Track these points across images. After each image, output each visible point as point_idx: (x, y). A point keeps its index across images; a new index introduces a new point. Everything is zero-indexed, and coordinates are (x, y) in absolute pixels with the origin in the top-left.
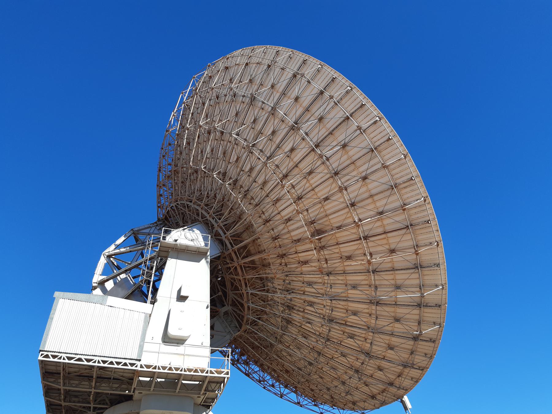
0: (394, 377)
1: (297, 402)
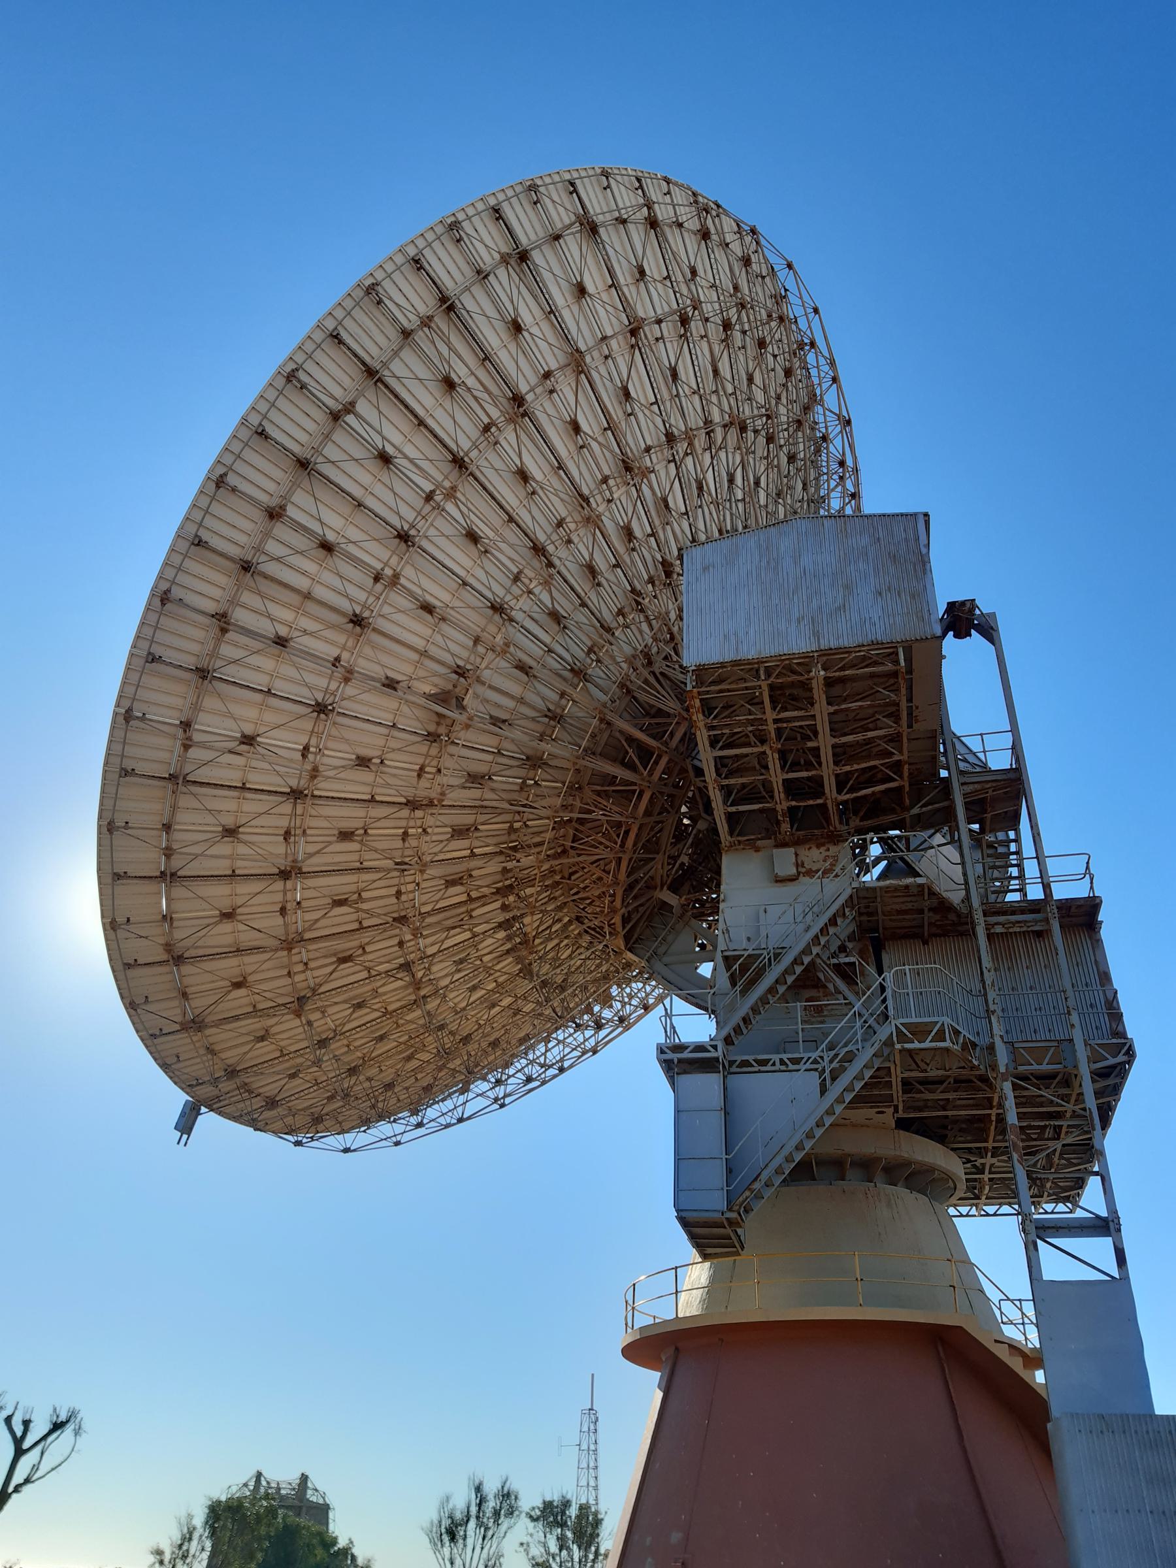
1: (835, 385)
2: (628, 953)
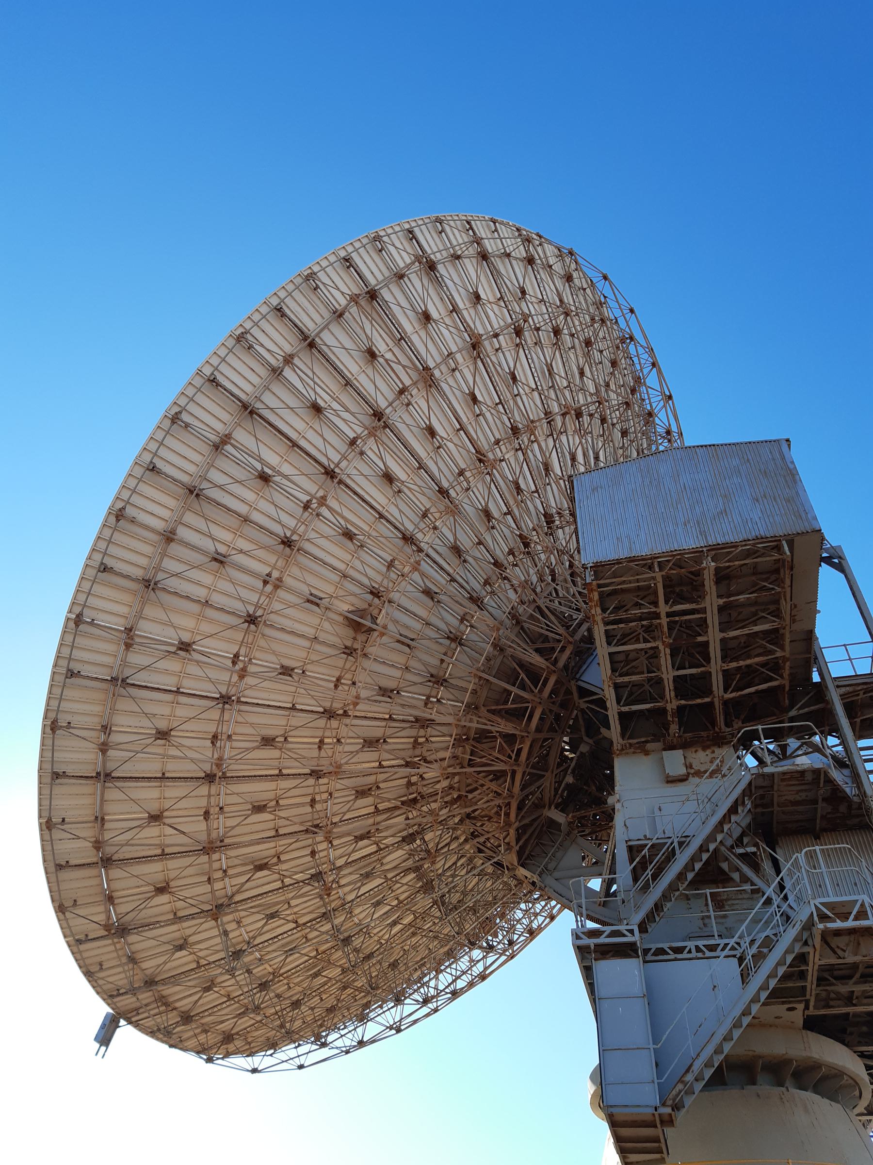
0: (467, 261)
2: (520, 868)
